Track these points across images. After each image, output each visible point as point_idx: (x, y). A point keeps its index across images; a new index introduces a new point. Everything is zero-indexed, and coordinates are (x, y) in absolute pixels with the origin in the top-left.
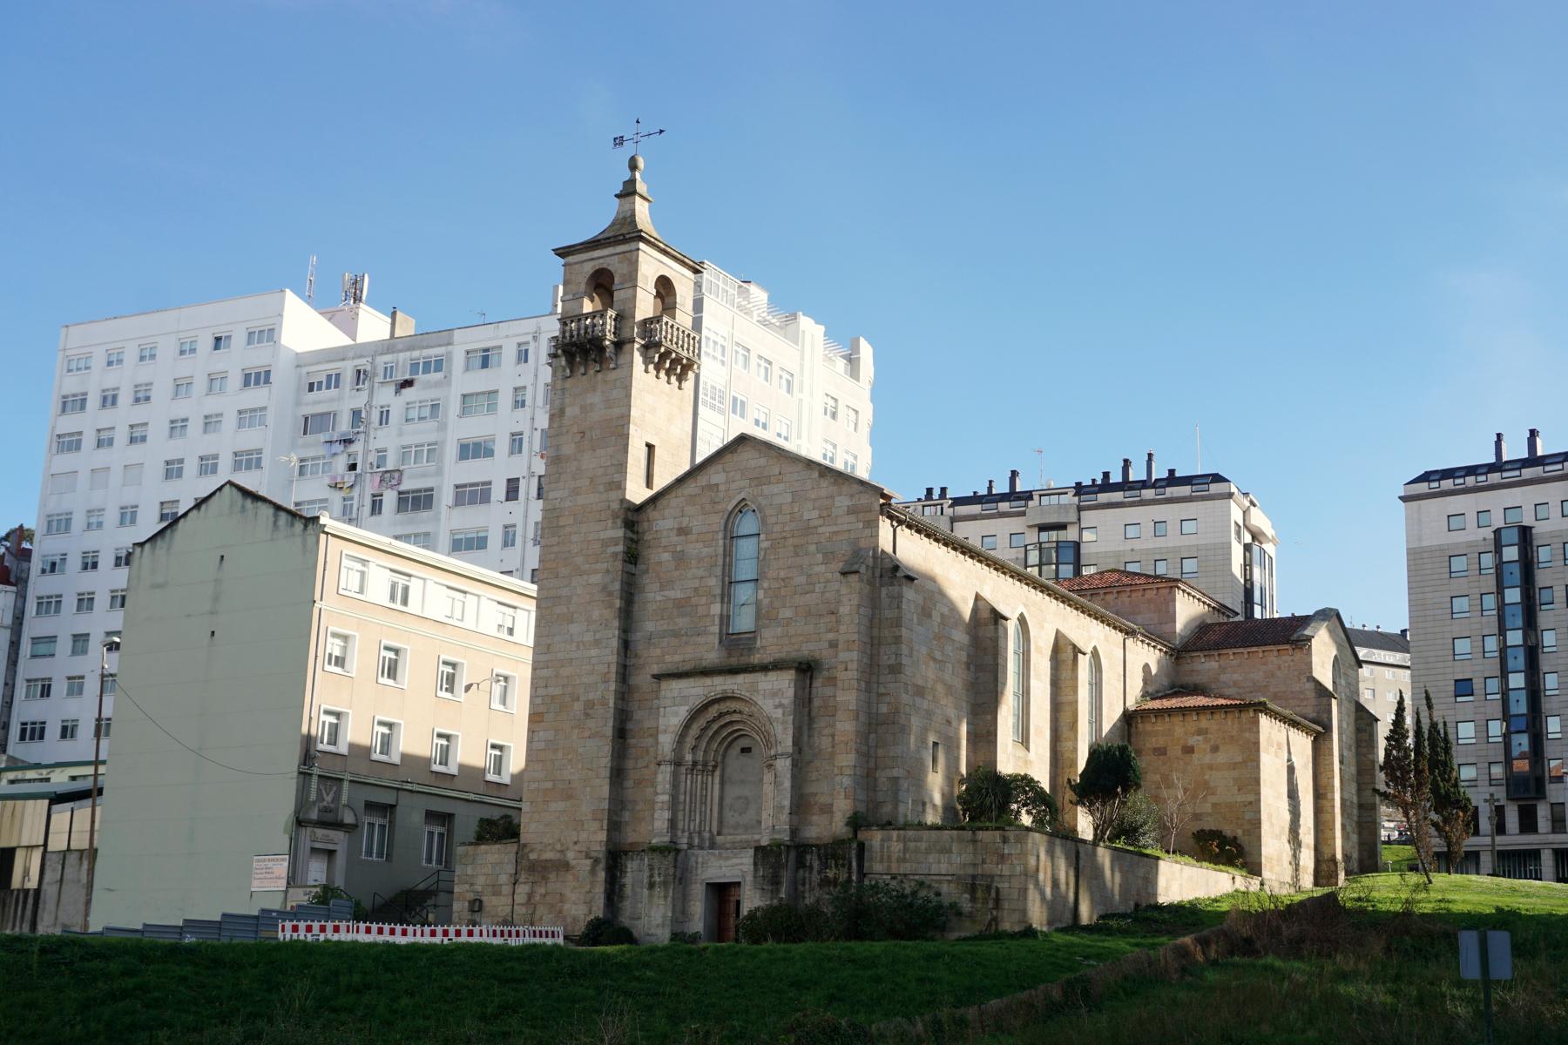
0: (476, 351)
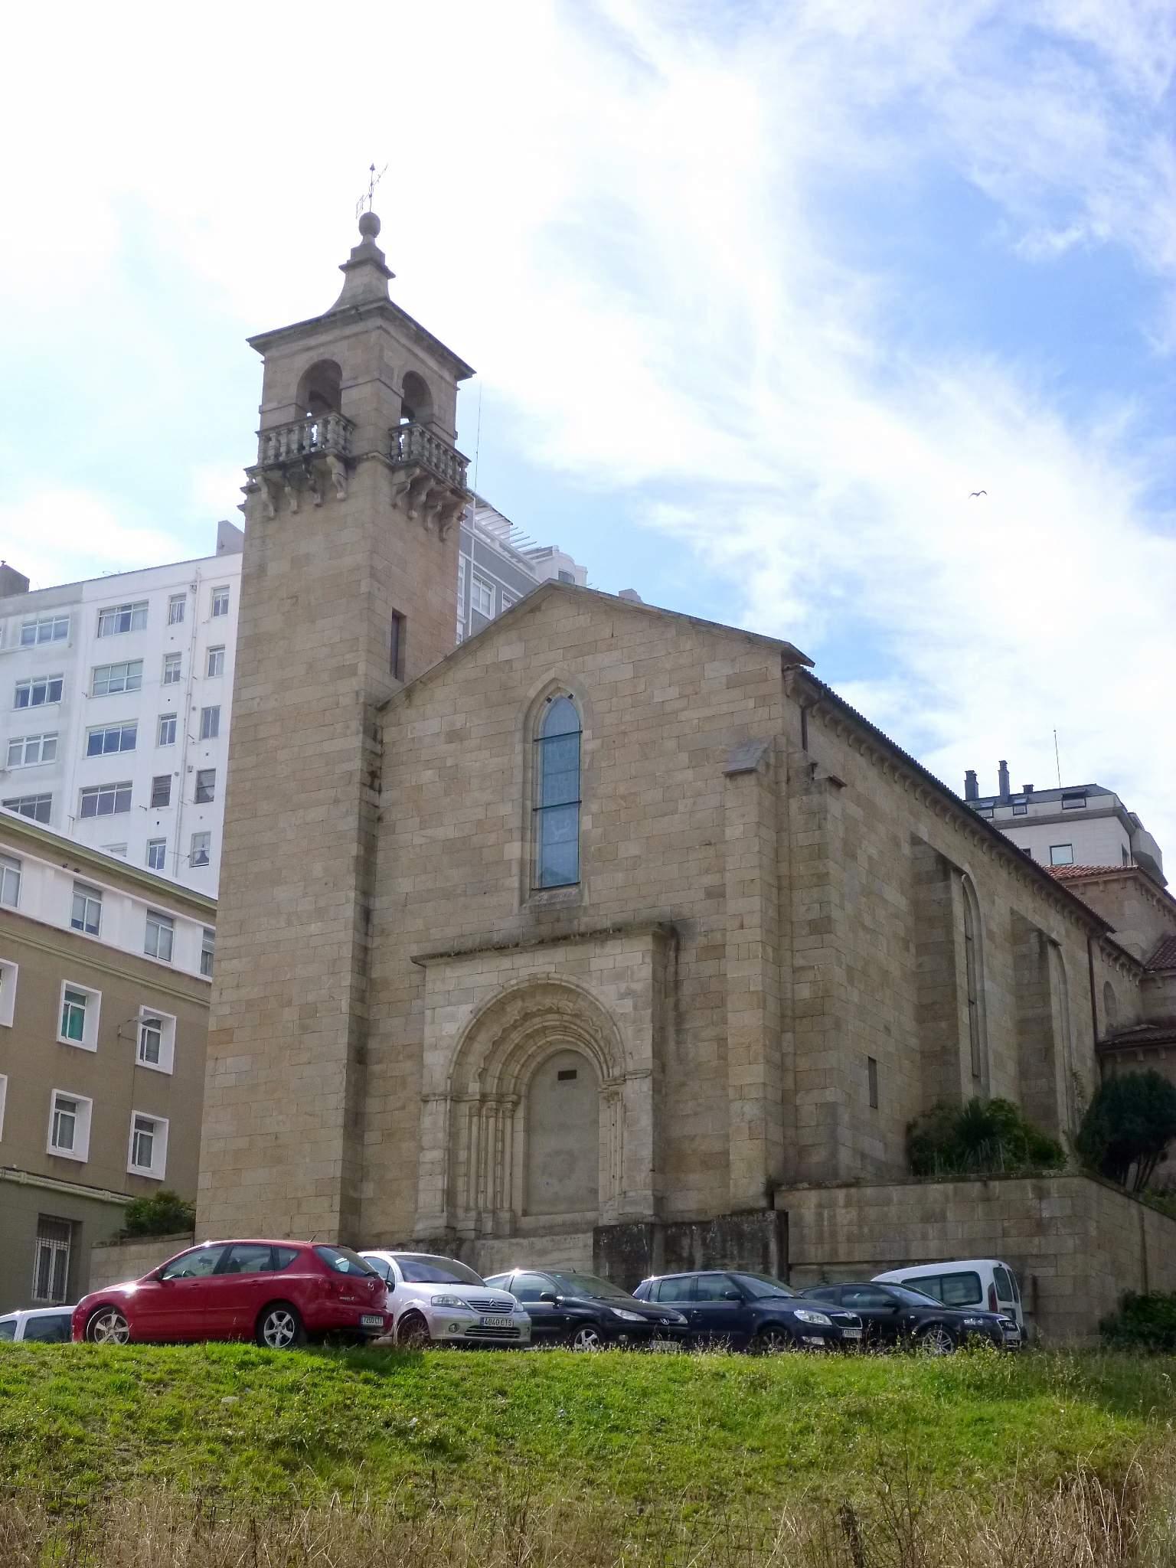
0: (111, 609)
